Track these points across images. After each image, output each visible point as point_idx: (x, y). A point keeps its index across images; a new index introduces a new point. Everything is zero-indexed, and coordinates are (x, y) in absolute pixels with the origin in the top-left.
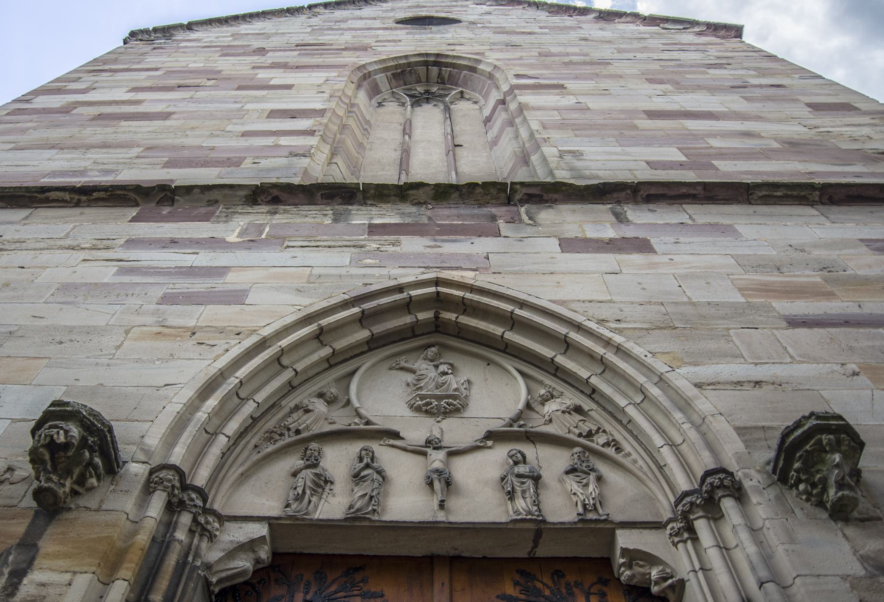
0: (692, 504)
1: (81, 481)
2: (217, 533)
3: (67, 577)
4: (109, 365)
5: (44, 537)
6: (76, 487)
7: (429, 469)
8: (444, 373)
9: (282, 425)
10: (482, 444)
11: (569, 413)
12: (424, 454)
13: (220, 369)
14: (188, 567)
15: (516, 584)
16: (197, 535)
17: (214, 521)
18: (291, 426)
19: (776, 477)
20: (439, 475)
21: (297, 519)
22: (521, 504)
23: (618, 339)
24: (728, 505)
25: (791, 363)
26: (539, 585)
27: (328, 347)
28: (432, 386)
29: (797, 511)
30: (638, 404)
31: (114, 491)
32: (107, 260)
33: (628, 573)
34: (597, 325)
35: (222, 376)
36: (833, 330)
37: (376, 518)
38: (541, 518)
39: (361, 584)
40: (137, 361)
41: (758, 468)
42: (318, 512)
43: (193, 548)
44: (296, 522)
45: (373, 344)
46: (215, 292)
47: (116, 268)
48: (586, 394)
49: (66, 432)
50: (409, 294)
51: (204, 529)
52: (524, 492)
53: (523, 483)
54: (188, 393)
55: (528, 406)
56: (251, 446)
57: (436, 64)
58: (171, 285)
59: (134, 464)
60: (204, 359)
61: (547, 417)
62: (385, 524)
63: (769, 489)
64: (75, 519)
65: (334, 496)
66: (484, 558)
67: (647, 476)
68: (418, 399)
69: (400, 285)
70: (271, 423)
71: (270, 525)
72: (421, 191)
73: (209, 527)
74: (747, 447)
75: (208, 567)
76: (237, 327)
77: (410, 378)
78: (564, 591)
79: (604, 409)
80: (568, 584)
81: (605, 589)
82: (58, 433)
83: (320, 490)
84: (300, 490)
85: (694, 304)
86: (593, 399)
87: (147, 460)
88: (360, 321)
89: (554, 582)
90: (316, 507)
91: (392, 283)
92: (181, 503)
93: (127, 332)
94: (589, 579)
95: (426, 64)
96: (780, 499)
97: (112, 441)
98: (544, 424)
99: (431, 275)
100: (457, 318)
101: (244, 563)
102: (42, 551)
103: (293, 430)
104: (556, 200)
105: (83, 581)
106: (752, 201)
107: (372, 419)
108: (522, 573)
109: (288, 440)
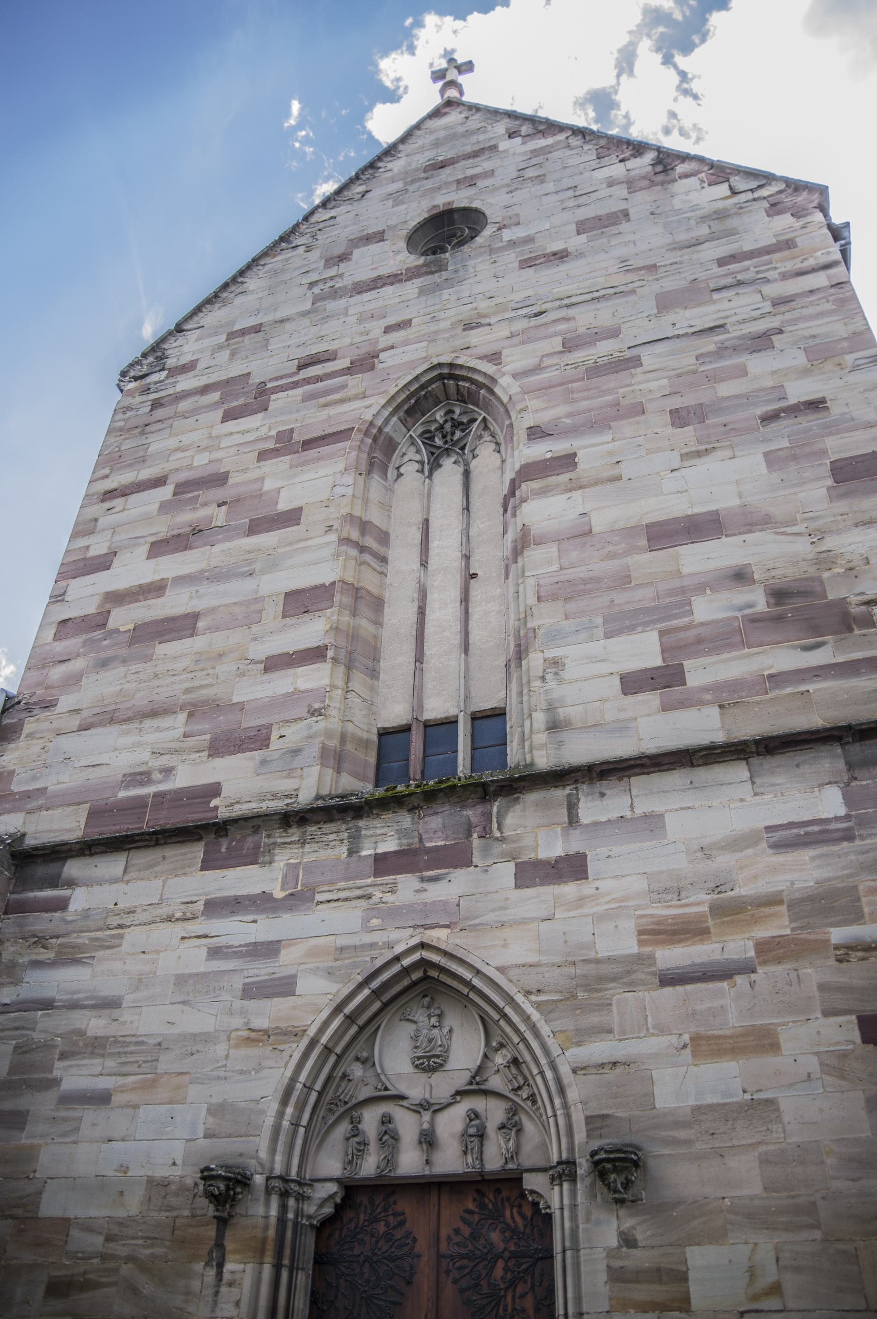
1: (233, 1200)
4: (225, 1078)
5: (226, 1238)
8: (434, 1027)
12: (419, 1112)
15: (474, 1200)
23: (535, 1016)
25: (645, 1037)
26: (486, 1200)
29: (599, 1195)
31: (251, 1200)
32: (198, 937)
35: (293, 1079)
36: (689, 987)
37: (392, 1174)
45: (385, 1005)
46: (275, 979)
47: (206, 949)
49: (218, 1188)
51: (303, 1196)
52: (472, 1149)
53: (472, 1142)
54: (275, 1106)
55: (486, 1056)
56: (320, 1119)
57: (451, 376)
61: (496, 1068)
70: (329, 1096)
72: (413, 798)
73: (305, 1195)
74: (588, 1136)
75: (309, 1217)
76: (294, 1027)
80: (502, 1199)
84: (350, 1157)
85: (597, 961)
89: (495, 1198)
90: (361, 1166)
91: (388, 955)
92: (287, 1191)
93: (229, 1039)
95: (441, 377)
96: (593, 1185)
99: (415, 941)
101: (328, 1210)
104: (524, 787)
105: (249, 1267)
106: (695, 763)
107: (389, 1086)
108: (478, 1191)
109: (342, 1110)
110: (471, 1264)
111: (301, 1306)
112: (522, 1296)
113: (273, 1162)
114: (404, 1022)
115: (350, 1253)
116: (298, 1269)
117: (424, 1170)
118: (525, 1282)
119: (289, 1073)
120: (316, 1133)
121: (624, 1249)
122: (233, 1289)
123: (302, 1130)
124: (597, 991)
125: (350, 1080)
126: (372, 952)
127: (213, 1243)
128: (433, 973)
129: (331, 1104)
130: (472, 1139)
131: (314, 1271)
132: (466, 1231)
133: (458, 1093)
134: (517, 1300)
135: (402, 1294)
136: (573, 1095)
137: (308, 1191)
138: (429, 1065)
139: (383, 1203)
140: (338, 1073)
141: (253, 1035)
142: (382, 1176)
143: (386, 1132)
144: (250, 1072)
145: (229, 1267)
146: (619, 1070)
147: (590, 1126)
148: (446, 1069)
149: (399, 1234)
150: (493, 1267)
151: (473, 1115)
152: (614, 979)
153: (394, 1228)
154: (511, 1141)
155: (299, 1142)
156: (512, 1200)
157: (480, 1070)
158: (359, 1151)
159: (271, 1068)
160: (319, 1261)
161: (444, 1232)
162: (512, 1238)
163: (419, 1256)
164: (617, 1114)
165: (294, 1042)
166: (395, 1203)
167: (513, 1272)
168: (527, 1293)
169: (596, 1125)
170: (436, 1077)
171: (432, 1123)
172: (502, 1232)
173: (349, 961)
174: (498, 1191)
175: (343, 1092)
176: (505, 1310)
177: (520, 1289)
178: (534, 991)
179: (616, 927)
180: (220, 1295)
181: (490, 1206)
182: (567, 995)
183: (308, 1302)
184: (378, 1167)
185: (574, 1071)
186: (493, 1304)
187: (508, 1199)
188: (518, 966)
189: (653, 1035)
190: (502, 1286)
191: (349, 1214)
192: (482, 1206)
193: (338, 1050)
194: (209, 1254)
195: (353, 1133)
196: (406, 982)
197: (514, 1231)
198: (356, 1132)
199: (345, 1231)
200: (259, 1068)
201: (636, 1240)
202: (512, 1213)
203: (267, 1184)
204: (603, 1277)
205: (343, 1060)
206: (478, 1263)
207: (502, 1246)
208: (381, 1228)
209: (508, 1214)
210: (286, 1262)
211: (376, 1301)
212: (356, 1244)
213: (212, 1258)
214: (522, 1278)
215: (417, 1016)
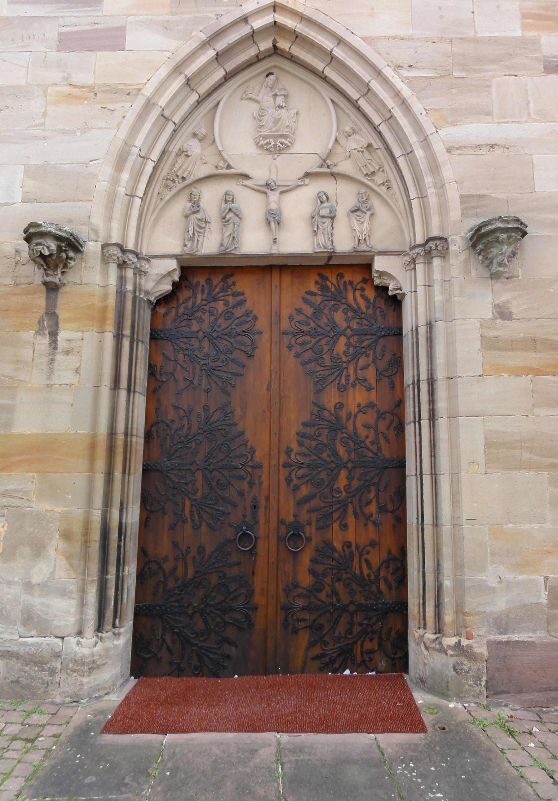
0: (418, 254)
1: (65, 266)
2: (148, 270)
3: (79, 334)
4: (44, 138)
5: (58, 306)
6: (64, 270)
7: (268, 208)
8: (281, 107)
9: (173, 171)
10: (302, 183)
11: (362, 152)
12: (265, 193)
13: (124, 140)
14: (138, 299)
15: (317, 283)
16: (138, 276)
17: (145, 264)
18: (178, 174)
19: (471, 243)
20: (274, 218)
22: (321, 239)
23: (406, 91)
24: (436, 262)
25: (526, 121)
26: (329, 284)
27: (195, 93)
28: (271, 125)
30: (408, 154)
34: (393, 73)
35: (127, 144)
38: (332, 251)
39: (232, 287)
40: (64, 132)
41: (463, 235)
42: (204, 248)
43: (137, 286)
45: (228, 77)
48: (377, 131)
49: (48, 247)
50: (252, 27)
51: (141, 271)
52: (324, 230)
53: (324, 223)
54: (108, 170)
58: (61, 20)
59: (91, 243)
60: (110, 129)
61: (348, 154)
63: (463, 253)
65: (211, 233)
67: (402, 215)
68: (261, 139)
69: (244, 15)
70: (164, 171)
71: (177, 259)
73: (143, 269)
74: (463, 215)
75: (147, 293)
76: (126, 85)
77: (255, 107)
78: (342, 287)
81: (365, 286)
82: (43, 248)
83: (202, 231)
84: (191, 233)
85: (476, 41)
87: (97, 239)
88: (216, 59)
92: (124, 262)
94: (357, 278)
96: (466, 262)
97: (75, 239)
98: (345, 160)
100: (290, 48)
101: (167, 287)
102: (60, 317)
103: (180, 177)
107: (232, 164)
108: (320, 275)
109: (180, 186)
110: (314, 341)
111: (142, 377)
113: (109, 230)
114: (244, 102)
115: (188, 330)
116: (138, 341)
117: (271, 249)
118: (368, 356)
119: (123, 134)
120: (151, 208)
121: (499, 321)
122: (70, 357)
123: (138, 201)
124: (475, 71)
125: (188, 156)
126: (217, 8)
127: (43, 311)
128: (284, 45)
129: (167, 179)
130: (325, 220)
131: (150, 346)
132: (309, 311)
133: (307, 175)
134: (359, 372)
135: (244, 367)
136: (447, 173)
137: (145, 266)
138: (275, 145)
139: (221, 284)
140: (174, 148)
141: (75, 91)
142: (226, 254)
143: (230, 210)
144: (74, 133)
145: (62, 335)
146: (498, 151)
147: (464, 206)
148: (294, 150)
150: (335, 343)
151: (324, 198)
152: (494, 61)
153: (233, 308)
154: (366, 224)
155: (135, 213)
156: (354, 284)
157: (330, 153)
158: (201, 228)
159: (101, 128)
160: (154, 337)
161: (285, 313)
162: (354, 318)
163: (260, 333)
164: (494, 195)
165: (126, 101)
166: (234, 284)
167: (355, 347)
169: (471, 204)
170: (281, 159)
171: (279, 203)
172: (345, 312)
173: (189, 16)
174: (341, 276)
175: (180, 168)
176: (347, 380)
177: (362, 361)
178: (405, 66)
179: (498, 7)
180: (56, 363)
181: (333, 289)
182: (442, 73)
183: (147, 374)
184: (222, 245)
185: (449, 151)
186: (336, 374)
187: (351, 283)
188: (387, 38)
189: (535, 120)
190: (344, 359)
191: (184, 294)
192: (324, 288)
193: (177, 118)
194: (39, 322)
195: (193, 210)
196: (252, 52)
197: (357, 312)
198: (196, 208)
199: (181, 310)
200: (86, 129)
201: (511, 313)
202: (354, 296)
203: (103, 253)
204: (478, 345)
205: (178, 136)
206: (321, 339)
207: (344, 325)
208: (220, 307)
209: (350, 296)
210: (127, 332)
211: (217, 373)
212: (194, 321)
213: (44, 327)
214: (365, 352)
215: (261, 95)
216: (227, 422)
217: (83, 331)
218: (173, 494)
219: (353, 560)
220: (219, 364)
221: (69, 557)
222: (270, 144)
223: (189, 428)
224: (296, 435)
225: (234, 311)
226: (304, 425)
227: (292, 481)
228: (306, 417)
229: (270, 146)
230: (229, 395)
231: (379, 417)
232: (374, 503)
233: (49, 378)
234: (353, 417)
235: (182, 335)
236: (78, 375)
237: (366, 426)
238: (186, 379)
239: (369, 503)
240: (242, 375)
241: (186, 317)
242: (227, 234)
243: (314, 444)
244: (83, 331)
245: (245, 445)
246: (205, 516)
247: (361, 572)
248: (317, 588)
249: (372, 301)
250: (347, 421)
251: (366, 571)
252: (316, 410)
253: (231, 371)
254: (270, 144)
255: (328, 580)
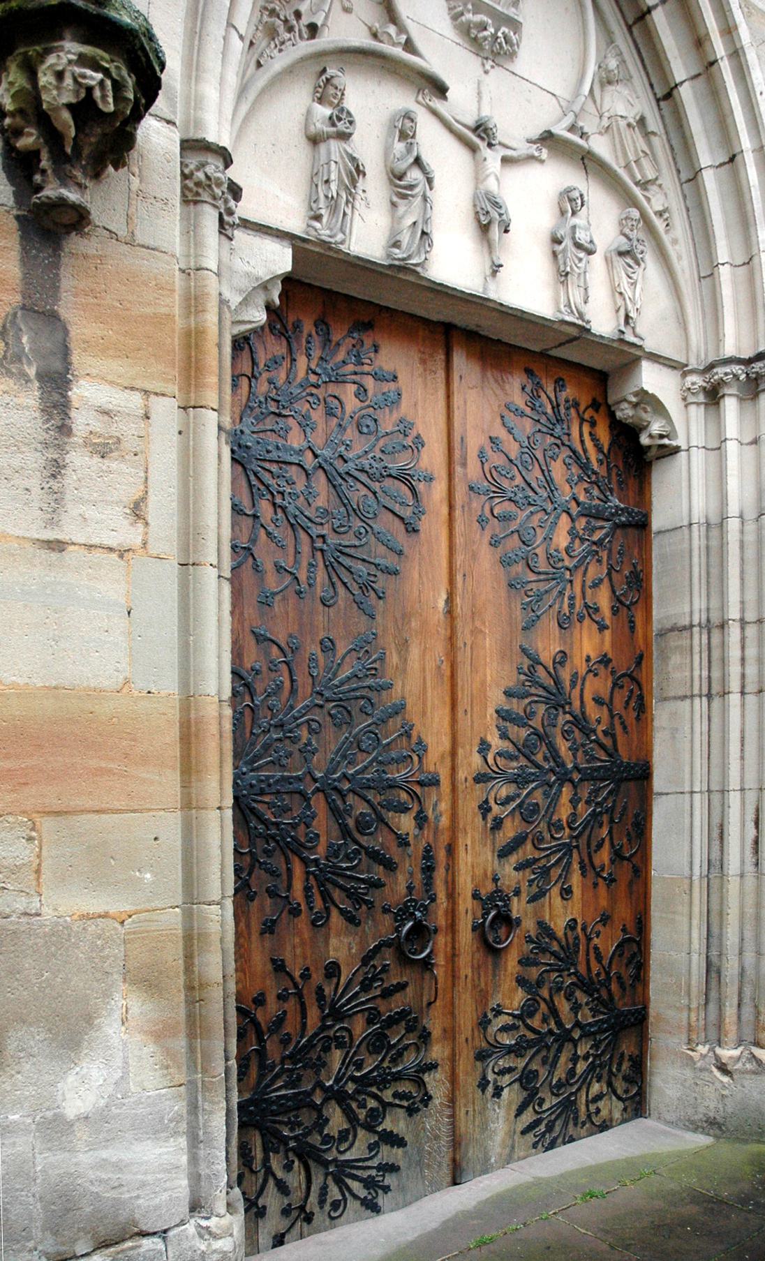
0: (736, 376)
3: (136, 399)
12: (473, 149)
21: (330, 249)
33: (630, 412)
44: (327, 253)
61: (605, 123)
62: (432, 286)
64: (100, 257)
66: (499, 341)
68: (470, 7)
79: (669, 141)
86: (659, 105)
102: (74, 332)
103: (305, 20)
105: (166, 410)
112: (595, 585)
134: (589, 592)
135: (400, 553)
149: (388, 422)
156: (582, 408)
168: (601, 580)
180: (70, 478)
216: (370, 682)
217: (146, 392)
218: (266, 851)
219: (578, 952)
220: (349, 540)
221: (160, 1034)
222: (485, 29)
223: (293, 691)
224: (495, 715)
225: (379, 415)
226: (508, 694)
227: (489, 810)
228: (510, 679)
229: (486, 33)
230: (372, 617)
231: (615, 684)
232: (607, 845)
233: (52, 523)
234: (579, 682)
235: (268, 452)
236: (140, 526)
237: (598, 701)
238: (279, 568)
239: (600, 845)
240: (396, 573)
241: (273, 407)
242: (409, 221)
243: (524, 733)
244: (146, 392)
245: (408, 735)
246: (337, 894)
247: (589, 969)
248: (528, 1011)
249: (606, 451)
250: (571, 689)
251: (595, 968)
252: (527, 662)
253: (377, 561)
254: (485, 29)
255: (545, 993)
